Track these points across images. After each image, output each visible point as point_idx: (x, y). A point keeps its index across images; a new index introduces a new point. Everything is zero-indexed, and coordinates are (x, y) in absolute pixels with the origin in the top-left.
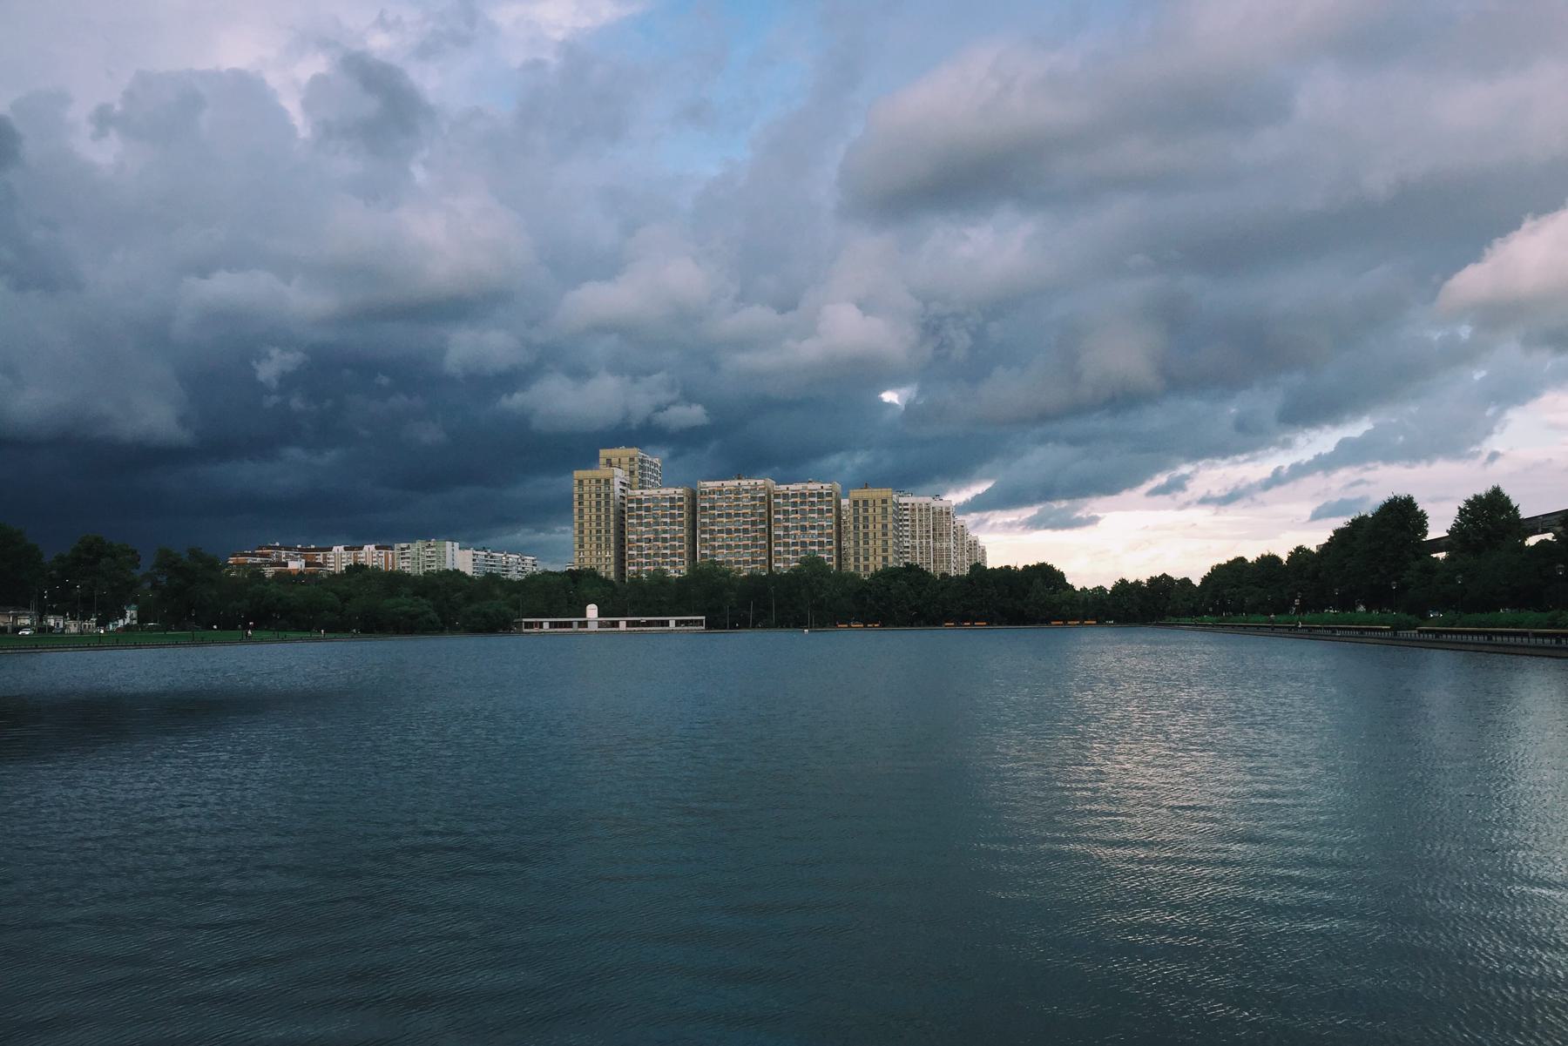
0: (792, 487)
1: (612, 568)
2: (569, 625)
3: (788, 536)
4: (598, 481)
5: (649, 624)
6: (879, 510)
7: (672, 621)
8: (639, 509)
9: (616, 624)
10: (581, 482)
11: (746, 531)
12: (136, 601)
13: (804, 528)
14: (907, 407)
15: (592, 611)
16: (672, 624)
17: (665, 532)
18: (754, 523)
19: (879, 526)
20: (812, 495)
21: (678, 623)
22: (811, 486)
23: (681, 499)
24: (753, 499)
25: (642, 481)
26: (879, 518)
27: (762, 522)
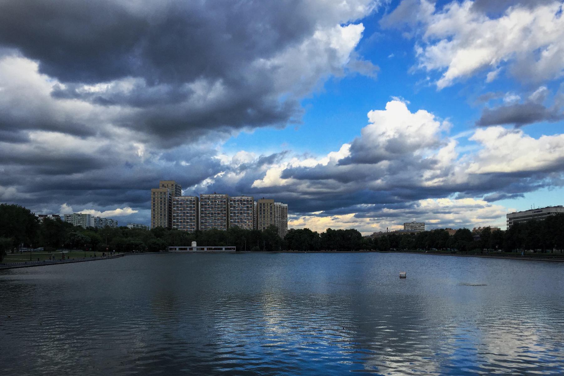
0: (237, 198)
1: (166, 223)
2: (185, 249)
3: (235, 216)
4: (161, 193)
5: (215, 249)
6: (269, 207)
7: (224, 248)
8: (177, 204)
9: (203, 249)
10: (154, 193)
11: (219, 214)
12: (284, 217)
13: (241, 213)
14: (505, 93)
15: (194, 244)
16: (224, 249)
17: (188, 213)
18: (221, 211)
19: (269, 213)
20: (244, 201)
21: (226, 249)
22: (243, 198)
23: (194, 201)
24: (221, 202)
25: (176, 193)
26: (269, 210)
27: (225, 210)
